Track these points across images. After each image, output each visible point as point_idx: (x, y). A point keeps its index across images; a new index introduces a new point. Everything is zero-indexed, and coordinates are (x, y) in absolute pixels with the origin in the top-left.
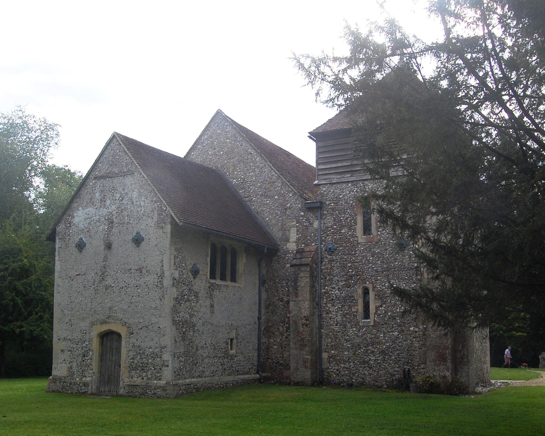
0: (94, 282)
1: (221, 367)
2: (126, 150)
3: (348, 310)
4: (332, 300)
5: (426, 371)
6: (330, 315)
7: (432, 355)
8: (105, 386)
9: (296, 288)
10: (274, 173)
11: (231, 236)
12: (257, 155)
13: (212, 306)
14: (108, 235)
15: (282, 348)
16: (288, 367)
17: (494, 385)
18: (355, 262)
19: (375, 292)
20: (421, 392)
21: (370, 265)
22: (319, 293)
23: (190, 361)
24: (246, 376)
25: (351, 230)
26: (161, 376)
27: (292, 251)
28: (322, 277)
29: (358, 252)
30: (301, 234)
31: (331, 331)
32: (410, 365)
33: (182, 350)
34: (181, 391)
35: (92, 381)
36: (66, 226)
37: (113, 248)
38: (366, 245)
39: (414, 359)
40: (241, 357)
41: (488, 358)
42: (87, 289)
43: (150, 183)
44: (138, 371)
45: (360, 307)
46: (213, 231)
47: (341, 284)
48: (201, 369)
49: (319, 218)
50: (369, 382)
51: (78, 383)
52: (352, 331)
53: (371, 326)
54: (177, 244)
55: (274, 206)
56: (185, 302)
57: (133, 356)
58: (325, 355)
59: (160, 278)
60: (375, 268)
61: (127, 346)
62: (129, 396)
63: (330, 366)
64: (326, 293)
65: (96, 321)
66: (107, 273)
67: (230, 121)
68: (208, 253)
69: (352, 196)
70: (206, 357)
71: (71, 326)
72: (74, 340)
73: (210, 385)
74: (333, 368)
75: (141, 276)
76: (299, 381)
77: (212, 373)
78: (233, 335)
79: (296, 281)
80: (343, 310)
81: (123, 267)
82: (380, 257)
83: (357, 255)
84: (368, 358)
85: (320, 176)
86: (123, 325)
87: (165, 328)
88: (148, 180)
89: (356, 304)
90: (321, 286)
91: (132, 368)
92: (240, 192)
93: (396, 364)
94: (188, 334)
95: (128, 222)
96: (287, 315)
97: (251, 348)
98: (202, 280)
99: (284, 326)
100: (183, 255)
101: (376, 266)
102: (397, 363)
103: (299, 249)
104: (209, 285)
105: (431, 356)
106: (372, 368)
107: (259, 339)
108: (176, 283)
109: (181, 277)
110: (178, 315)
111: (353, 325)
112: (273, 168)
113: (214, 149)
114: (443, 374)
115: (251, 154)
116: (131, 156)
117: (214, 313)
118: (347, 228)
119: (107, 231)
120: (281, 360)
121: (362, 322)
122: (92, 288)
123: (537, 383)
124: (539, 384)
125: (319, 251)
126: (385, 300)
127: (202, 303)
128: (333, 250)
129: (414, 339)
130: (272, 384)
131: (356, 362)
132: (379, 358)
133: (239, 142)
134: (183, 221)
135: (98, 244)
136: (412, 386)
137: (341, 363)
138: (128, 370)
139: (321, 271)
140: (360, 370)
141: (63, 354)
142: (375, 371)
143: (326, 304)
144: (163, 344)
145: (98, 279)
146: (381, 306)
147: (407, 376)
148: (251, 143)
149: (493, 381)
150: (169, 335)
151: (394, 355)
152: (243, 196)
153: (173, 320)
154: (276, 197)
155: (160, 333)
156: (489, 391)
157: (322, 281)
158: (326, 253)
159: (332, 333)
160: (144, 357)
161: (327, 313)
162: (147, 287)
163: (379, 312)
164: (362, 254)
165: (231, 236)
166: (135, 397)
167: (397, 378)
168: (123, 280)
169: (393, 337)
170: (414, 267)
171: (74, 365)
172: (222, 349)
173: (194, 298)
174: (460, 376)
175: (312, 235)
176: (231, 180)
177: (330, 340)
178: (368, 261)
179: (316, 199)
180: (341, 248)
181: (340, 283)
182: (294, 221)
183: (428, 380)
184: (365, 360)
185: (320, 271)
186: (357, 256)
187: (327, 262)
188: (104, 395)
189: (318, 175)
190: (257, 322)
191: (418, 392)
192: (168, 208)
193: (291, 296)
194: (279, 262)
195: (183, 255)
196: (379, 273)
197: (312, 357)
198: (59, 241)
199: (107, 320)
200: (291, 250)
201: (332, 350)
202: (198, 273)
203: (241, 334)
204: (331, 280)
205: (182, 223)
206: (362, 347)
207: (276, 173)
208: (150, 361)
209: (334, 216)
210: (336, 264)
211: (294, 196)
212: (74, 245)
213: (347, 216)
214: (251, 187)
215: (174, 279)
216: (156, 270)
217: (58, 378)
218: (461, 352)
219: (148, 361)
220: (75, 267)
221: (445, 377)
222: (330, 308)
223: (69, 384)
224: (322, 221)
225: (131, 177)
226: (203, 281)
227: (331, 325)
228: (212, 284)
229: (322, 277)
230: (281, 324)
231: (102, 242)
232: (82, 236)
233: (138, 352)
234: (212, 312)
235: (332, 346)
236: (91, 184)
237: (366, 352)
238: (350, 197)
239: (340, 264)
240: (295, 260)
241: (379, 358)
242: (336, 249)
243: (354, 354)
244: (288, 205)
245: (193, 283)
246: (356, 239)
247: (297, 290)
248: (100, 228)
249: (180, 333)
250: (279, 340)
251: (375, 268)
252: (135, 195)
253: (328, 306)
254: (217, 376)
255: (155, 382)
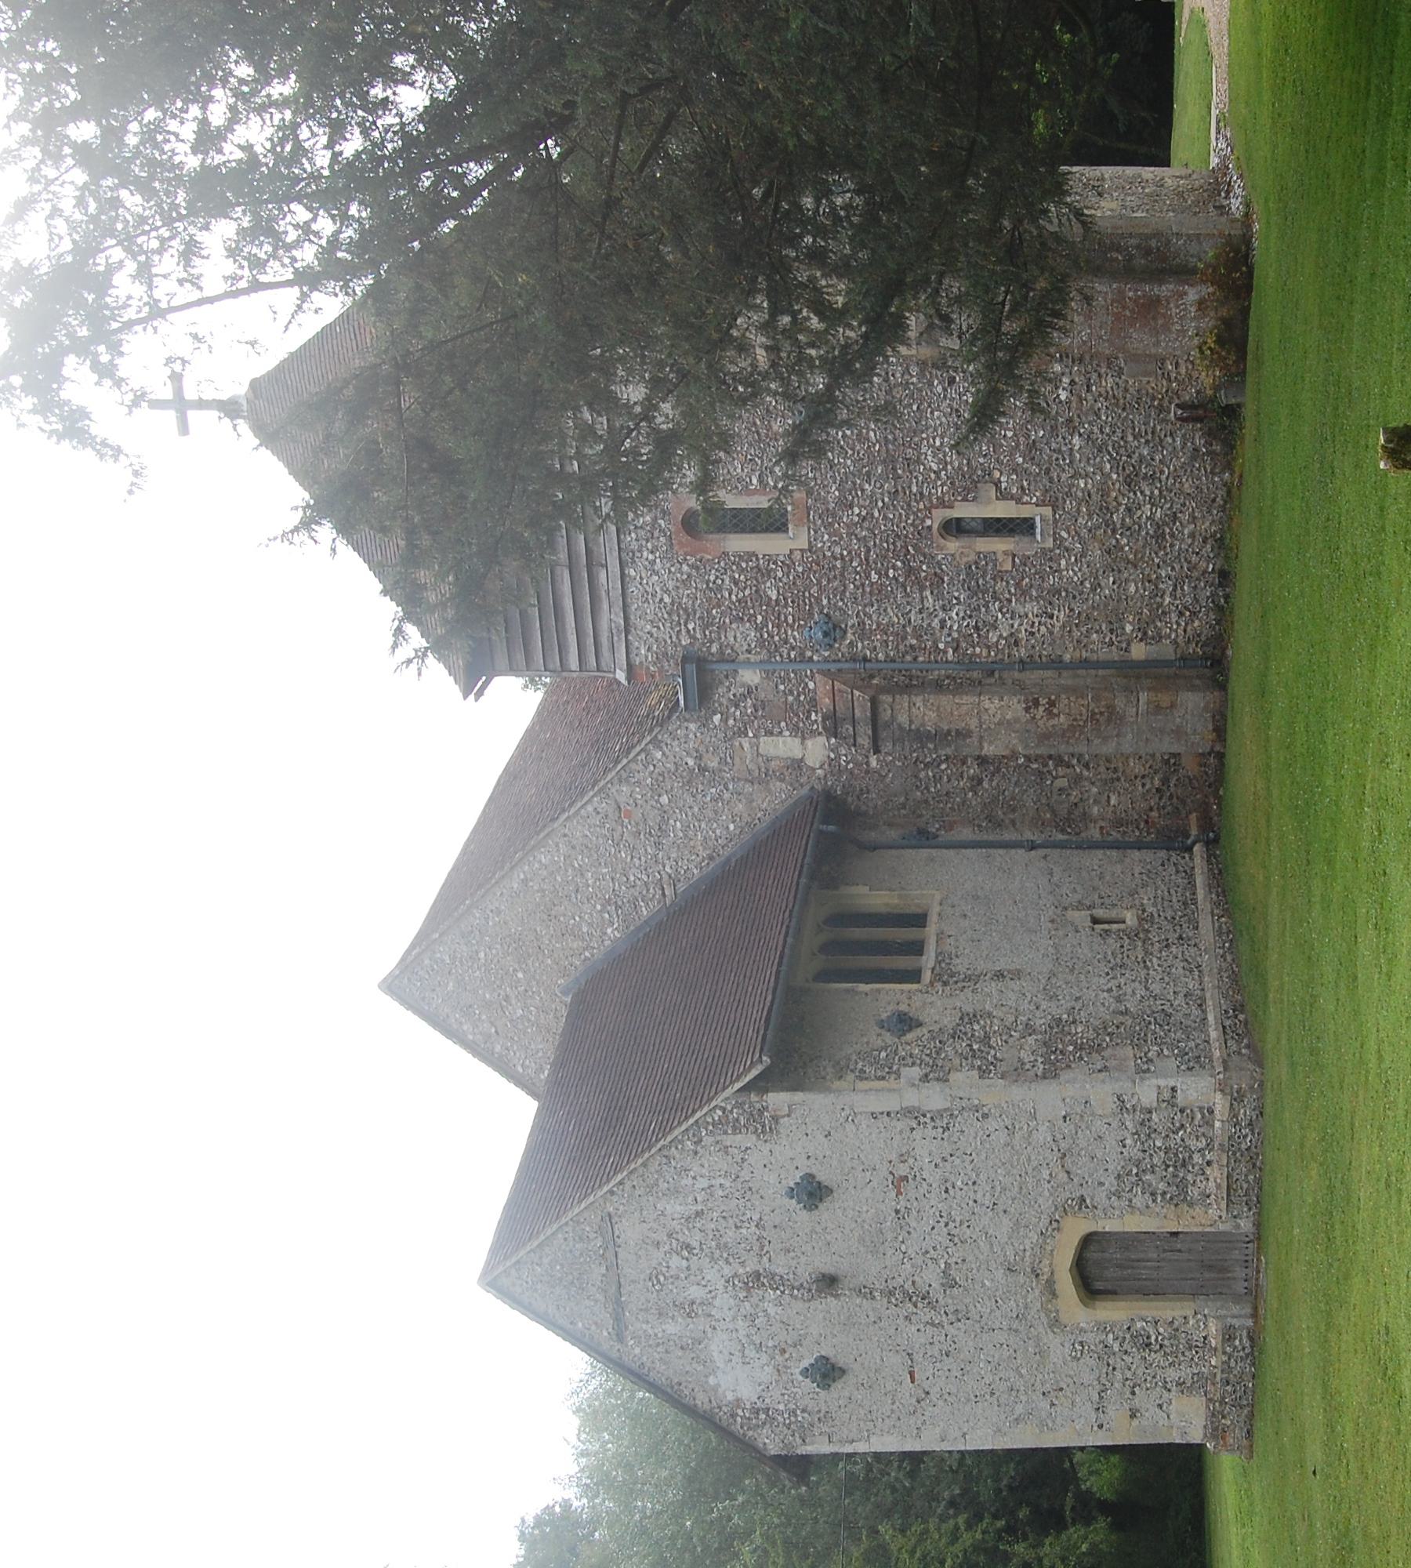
0: (933, 1324)
1: (1174, 949)
2: (536, 1243)
3: (1008, 582)
4: (977, 628)
5: (1185, 358)
6: (1023, 635)
7: (1139, 339)
8: (1234, 1279)
9: (942, 737)
10: (590, 808)
11: (793, 924)
12: (530, 862)
13: (1000, 975)
14: (793, 1288)
15: (1118, 779)
16: (1172, 761)
17: (1224, 160)
18: (867, 560)
19: (956, 500)
20: (1243, 373)
21: (876, 514)
22: (957, 667)
23: (1158, 1030)
24: (1200, 880)
25: (769, 572)
26: (1201, 1109)
27: (832, 750)
28: (908, 658)
29: (838, 550)
30: (779, 722)
31: (1070, 632)
32: (1166, 403)
33: (1129, 1051)
34: (1243, 1051)
35: (1217, 1318)
36: (764, 1424)
37: (832, 1271)
38: (815, 524)
39: (1151, 391)
40: (1146, 898)
41: (1148, 172)
42: (953, 1346)
43: (640, 1161)
44: (1190, 1177)
45: (999, 546)
46: (782, 973)
47: (931, 600)
48: (1179, 1001)
49: (732, 666)
50: (1213, 521)
51: (1225, 1358)
52: (1070, 571)
53: (1054, 516)
54: (823, 1073)
55: (690, 807)
56: (990, 1047)
57: (1147, 1195)
58: (1138, 651)
59: (922, 1120)
60: (886, 499)
61: (1117, 1213)
62: (1258, 1202)
63: (1170, 637)
64: (958, 646)
65: (1048, 1312)
66: (908, 1286)
67: (417, 950)
68: (847, 991)
69: (668, 565)
70: (1147, 989)
71: (1061, 1389)
72: (1104, 1381)
73: (1225, 975)
74: (1175, 627)
75: (918, 1178)
76: (1211, 727)
77: (1191, 971)
78: (1081, 917)
79: (921, 737)
80: (1008, 596)
81: (890, 1236)
82: (854, 483)
83: (845, 553)
84: (1146, 524)
85: (603, 664)
86: (1058, 1229)
87: (1068, 1100)
88: (633, 1166)
89: (990, 557)
90: (936, 662)
91: (1179, 1197)
92: (645, 913)
93: (1164, 443)
94: (1082, 1038)
95: (757, 1226)
96: (1020, 766)
97: (1118, 868)
98: (925, 1003)
99: (1054, 773)
100: (854, 1057)
101: (878, 496)
102: (1161, 441)
103: (823, 728)
104: (939, 986)
105: (1142, 341)
106: (1175, 513)
107: (1093, 846)
108: (936, 1072)
109: (918, 1062)
110: (1028, 1066)
111: (1050, 567)
112: (573, 810)
113: (507, 998)
114: (1193, 309)
115: (525, 881)
116: (555, 1226)
117: (1019, 971)
118: (764, 583)
119: (783, 1292)
120: (1152, 783)
121: (1043, 541)
122: (952, 1330)
123: (1220, 32)
124: (1224, 26)
125: (833, 667)
126: (979, 472)
127: (991, 1002)
128: (830, 625)
129: (1094, 388)
130: (1219, 806)
131: (1157, 560)
132: (1148, 493)
133: (487, 919)
134: (757, 1055)
135: (821, 1316)
136: (1226, 397)
137: (1160, 605)
138: (1186, 1208)
139: (893, 661)
140: (1180, 548)
141: (1143, 1411)
142: (1183, 505)
143: (989, 648)
144: (1111, 1104)
145: (926, 1314)
146: (997, 484)
147: (1196, 412)
148: (493, 881)
149: (1214, 161)
150: (1088, 1086)
151: (1137, 448)
152: (659, 903)
153: (1045, 1077)
154: (664, 799)
155: (1082, 1116)
156: (1241, 177)
157: (921, 659)
158: (837, 645)
159: (1074, 629)
160: (1148, 1160)
161: (1016, 643)
162: (950, 1159)
163: (1014, 491)
164: (841, 538)
165: (793, 924)
166: (1259, 1181)
167: (1202, 442)
168: (929, 1234)
169: (1087, 451)
170: (885, 384)
171: (1172, 1374)
172: (1122, 947)
173: (978, 1023)
174: (1200, 260)
175: (782, 687)
176: (607, 943)
177: (1095, 635)
178: (864, 519)
179: (673, 675)
180: (825, 602)
181: (927, 605)
182: (740, 744)
183: (1209, 352)
184: (1151, 532)
185: (892, 665)
186: (850, 553)
187: (866, 643)
188: (1257, 1279)
189: (598, 670)
190: (1041, 852)
191: (1244, 382)
192: (718, 1101)
193: (965, 751)
194: (862, 790)
195: (854, 1057)
196: (900, 488)
197: (1142, 689)
198: (812, 1443)
199: (1045, 1277)
200: (827, 753)
201: (1124, 629)
202: (905, 1014)
203: (1078, 897)
204: (918, 633)
205: (764, 1058)
206: (1114, 542)
207: (590, 801)
208: (1158, 1143)
209: (727, 621)
210: (870, 618)
211: (663, 745)
212: (823, 1393)
213: (727, 581)
214: (632, 878)
215: (925, 1078)
216: (901, 1132)
217: (1212, 1422)
218: (1132, 256)
219: (1159, 1148)
220: (889, 1388)
221: (1201, 304)
222: (1001, 636)
223: (1229, 1388)
224: (742, 657)
225: (619, 1225)
226: (929, 1000)
227: (1051, 633)
228: (937, 977)
229: (908, 658)
230: (1048, 782)
231: (815, 1304)
232: (798, 1371)
233: (1134, 1179)
234: (1017, 974)
235: (1112, 633)
236: (637, 1351)
237: (1129, 529)
238: (670, 571)
239: (872, 606)
240: (860, 740)
241: (1148, 493)
242: (826, 615)
243: (1135, 567)
244: (691, 762)
245: (936, 1028)
246: (797, 555)
247: (949, 732)
248: (773, 1314)
249: (1081, 1058)
250: (1095, 790)
251: (886, 499)
252: (675, 1208)
253: (995, 640)
254: (1199, 959)
255: (1217, 1124)
